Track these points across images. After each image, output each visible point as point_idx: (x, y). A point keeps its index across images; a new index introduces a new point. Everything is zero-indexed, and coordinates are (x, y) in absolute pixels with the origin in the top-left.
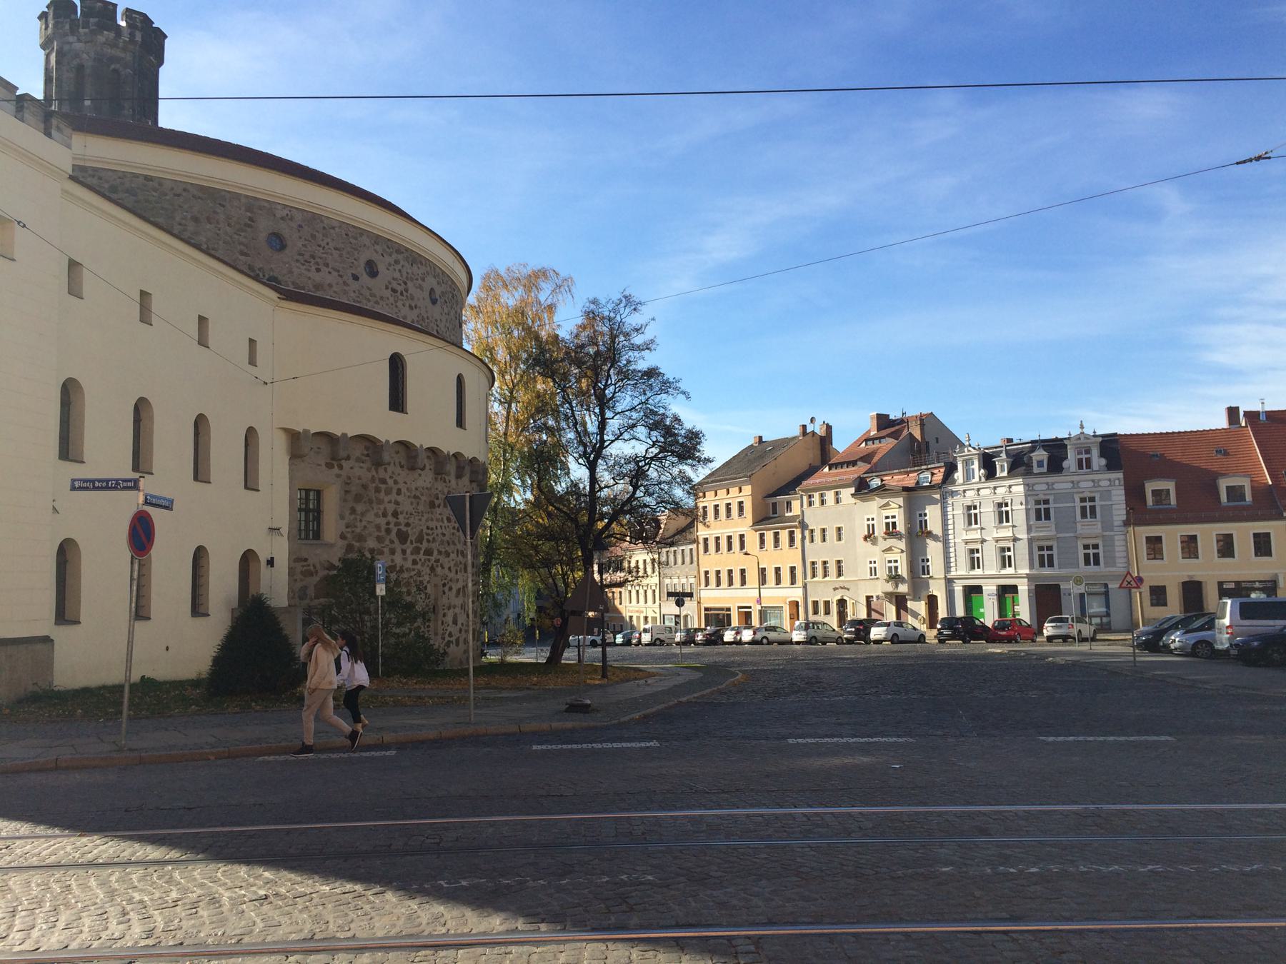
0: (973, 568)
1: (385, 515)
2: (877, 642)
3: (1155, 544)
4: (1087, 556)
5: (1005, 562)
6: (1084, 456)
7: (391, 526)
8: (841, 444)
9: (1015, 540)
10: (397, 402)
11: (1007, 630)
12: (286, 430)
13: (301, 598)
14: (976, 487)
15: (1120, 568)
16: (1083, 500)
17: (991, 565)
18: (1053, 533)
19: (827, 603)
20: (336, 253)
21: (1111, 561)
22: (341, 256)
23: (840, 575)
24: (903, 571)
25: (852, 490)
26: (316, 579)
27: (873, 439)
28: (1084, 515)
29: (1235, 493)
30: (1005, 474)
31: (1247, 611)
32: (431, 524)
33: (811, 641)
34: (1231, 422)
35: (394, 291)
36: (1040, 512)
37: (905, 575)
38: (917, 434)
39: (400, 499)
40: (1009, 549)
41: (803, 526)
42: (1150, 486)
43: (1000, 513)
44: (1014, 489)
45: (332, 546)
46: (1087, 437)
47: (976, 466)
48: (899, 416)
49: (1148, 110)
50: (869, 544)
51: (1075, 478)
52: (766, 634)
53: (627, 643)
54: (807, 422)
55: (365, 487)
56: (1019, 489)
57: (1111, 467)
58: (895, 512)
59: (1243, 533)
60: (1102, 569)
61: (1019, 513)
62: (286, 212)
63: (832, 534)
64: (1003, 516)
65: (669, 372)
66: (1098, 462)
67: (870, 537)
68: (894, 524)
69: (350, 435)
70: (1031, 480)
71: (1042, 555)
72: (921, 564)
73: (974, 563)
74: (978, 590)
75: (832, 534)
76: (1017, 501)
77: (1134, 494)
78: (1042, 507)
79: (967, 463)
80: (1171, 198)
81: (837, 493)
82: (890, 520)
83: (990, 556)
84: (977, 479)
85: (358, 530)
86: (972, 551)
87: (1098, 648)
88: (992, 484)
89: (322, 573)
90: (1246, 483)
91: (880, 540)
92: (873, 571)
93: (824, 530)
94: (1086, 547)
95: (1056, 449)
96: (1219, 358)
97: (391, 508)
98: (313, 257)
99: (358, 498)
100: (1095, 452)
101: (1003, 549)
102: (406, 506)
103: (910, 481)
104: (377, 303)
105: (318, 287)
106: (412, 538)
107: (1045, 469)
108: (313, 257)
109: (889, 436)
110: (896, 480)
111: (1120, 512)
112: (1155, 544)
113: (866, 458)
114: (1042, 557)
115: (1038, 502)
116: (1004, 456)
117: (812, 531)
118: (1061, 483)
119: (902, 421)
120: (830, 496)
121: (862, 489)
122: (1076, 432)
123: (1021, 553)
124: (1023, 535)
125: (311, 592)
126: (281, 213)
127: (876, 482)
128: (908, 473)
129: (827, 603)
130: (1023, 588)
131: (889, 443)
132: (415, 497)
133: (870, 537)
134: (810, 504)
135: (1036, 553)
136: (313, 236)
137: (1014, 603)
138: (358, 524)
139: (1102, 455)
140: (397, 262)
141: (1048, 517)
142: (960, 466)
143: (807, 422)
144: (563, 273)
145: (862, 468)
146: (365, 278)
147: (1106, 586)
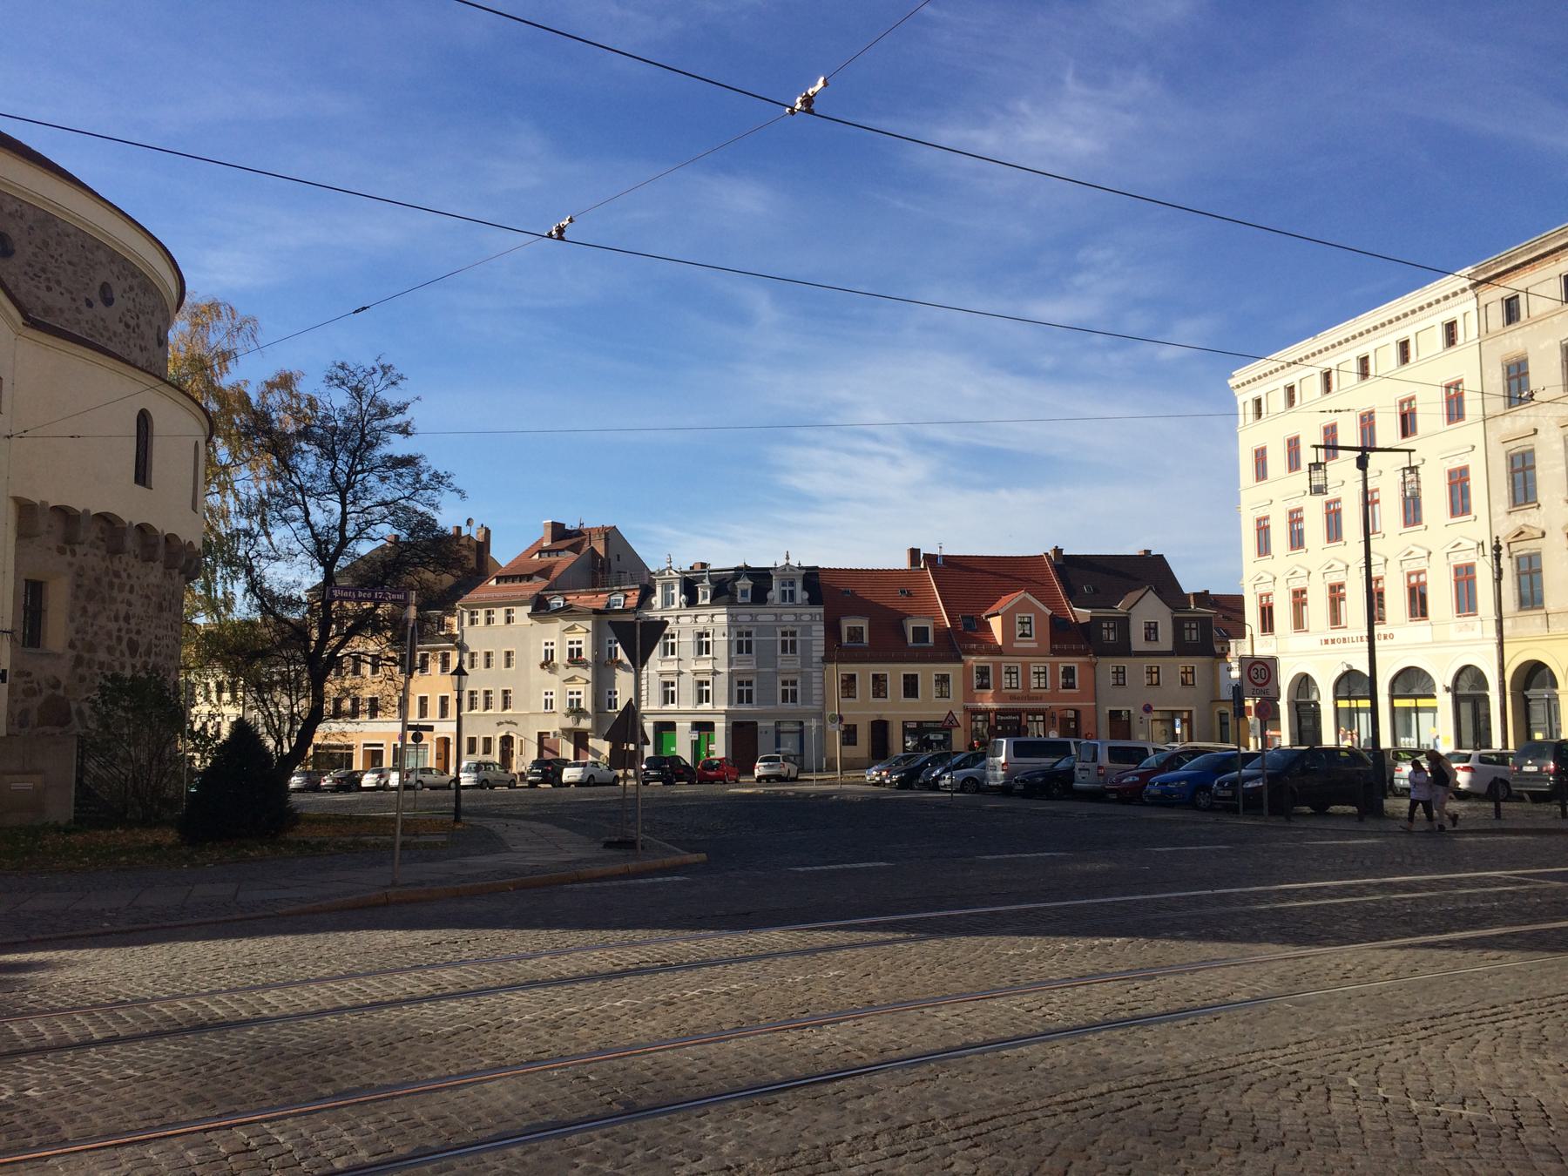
0: (666, 702)
1: (116, 619)
2: (568, 784)
3: (849, 683)
4: (785, 692)
5: (703, 697)
6: (788, 588)
7: (123, 633)
8: (503, 554)
9: (715, 673)
10: (142, 475)
11: (703, 771)
12: (16, 500)
13: (22, 725)
14: (676, 613)
15: (815, 706)
16: (784, 634)
17: (686, 701)
18: (753, 667)
19: (488, 741)
20: (69, 268)
21: (808, 699)
22: (75, 273)
23: (505, 707)
24: (587, 704)
25: (529, 609)
26: (38, 701)
27: (549, 551)
28: (784, 650)
29: (921, 633)
30: (707, 601)
31: (1020, 750)
32: (161, 632)
33: (481, 784)
34: (913, 563)
35: (127, 326)
36: (742, 644)
37: (589, 709)
38: (600, 548)
39: (133, 598)
40: (707, 683)
41: (462, 648)
42: (847, 624)
43: (700, 644)
44: (716, 618)
45: (59, 656)
46: (792, 568)
47: (676, 590)
48: (576, 526)
49: (743, 203)
50: (546, 672)
51: (779, 611)
52: (420, 777)
53: (339, 787)
54: (463, 524)
55: (98, 580)
56: (722, 618)
57: (813, 601)
58: (581, 637)
59: (926, 673)
60: (799, 706)
61: (720, 643)
62: (15, 206)
63: (498, 659)
64: (703, 647)
65: (434, 461)
66: (801, 595)
67: (548, 664)
68: (579, 650)
69: (93, 512)
70: (734, 611)
71: (742, 691)
72: (608, 697)
73: (668, 697)
74: (671, 726)
75: (498, 659)
76: (719, 631)
77: (832, 630)
78: (744, 639)
79: (667, 587)
80: (760, 301)
81: (508, 612)
82: (575, 646)
83: (686, 689)
84: (676, 605)
85: (88, 638)
86: (666, 684)
87: (798, 787)
88: (693, 612)
89: (47, 692)
90: (930, 625)
91: (562, 668)
92: (549, 704)
93: (488, 654)
94: (785, 683)
95: (761, 578)
96: (796, 482)
97: (123, 609)
98: (44, 270)
99: (90, 596)
100: (799, 585)
101: (701, 683)
102: (138, 609)
103: (600, 601)
104: (110, 339)
105: (48, 310)
106: (141, 650)
107: (749, 599)
108: (44, 270)
109: (568, 548)
110: (584, 600)
111: (818, 649)
112: (849, 683)
113: (544, 572)
114: (740, 693)
115: (740, 634)
116: (706, 581)
117: (473, 655)
118: (765, 615)
119: (579, 533)
120: (481, 615)
121: (541, 609)
122: (781, 563)
123: (721, 688)
124: (724, 669)
125: (34, 717)
126: (10, 207)
127: (557, 602)
128: (597, 593)
129: (488, 741)
130: (720, 725)
131: (568, 558)
132: (147, 597)
133: (548, 664)
134: (472, 622)
135: (736, 688)
136: (46, 244)
137: (709, 742)
138: (89, 630)
139: (804, 588)
140: (131, 288)
141: (749, 651)
142: (659, 590)
143: (463, 524)
144: (243, 311)
145: (539, 584)
146: (99, 306)
147: (801, 723)
